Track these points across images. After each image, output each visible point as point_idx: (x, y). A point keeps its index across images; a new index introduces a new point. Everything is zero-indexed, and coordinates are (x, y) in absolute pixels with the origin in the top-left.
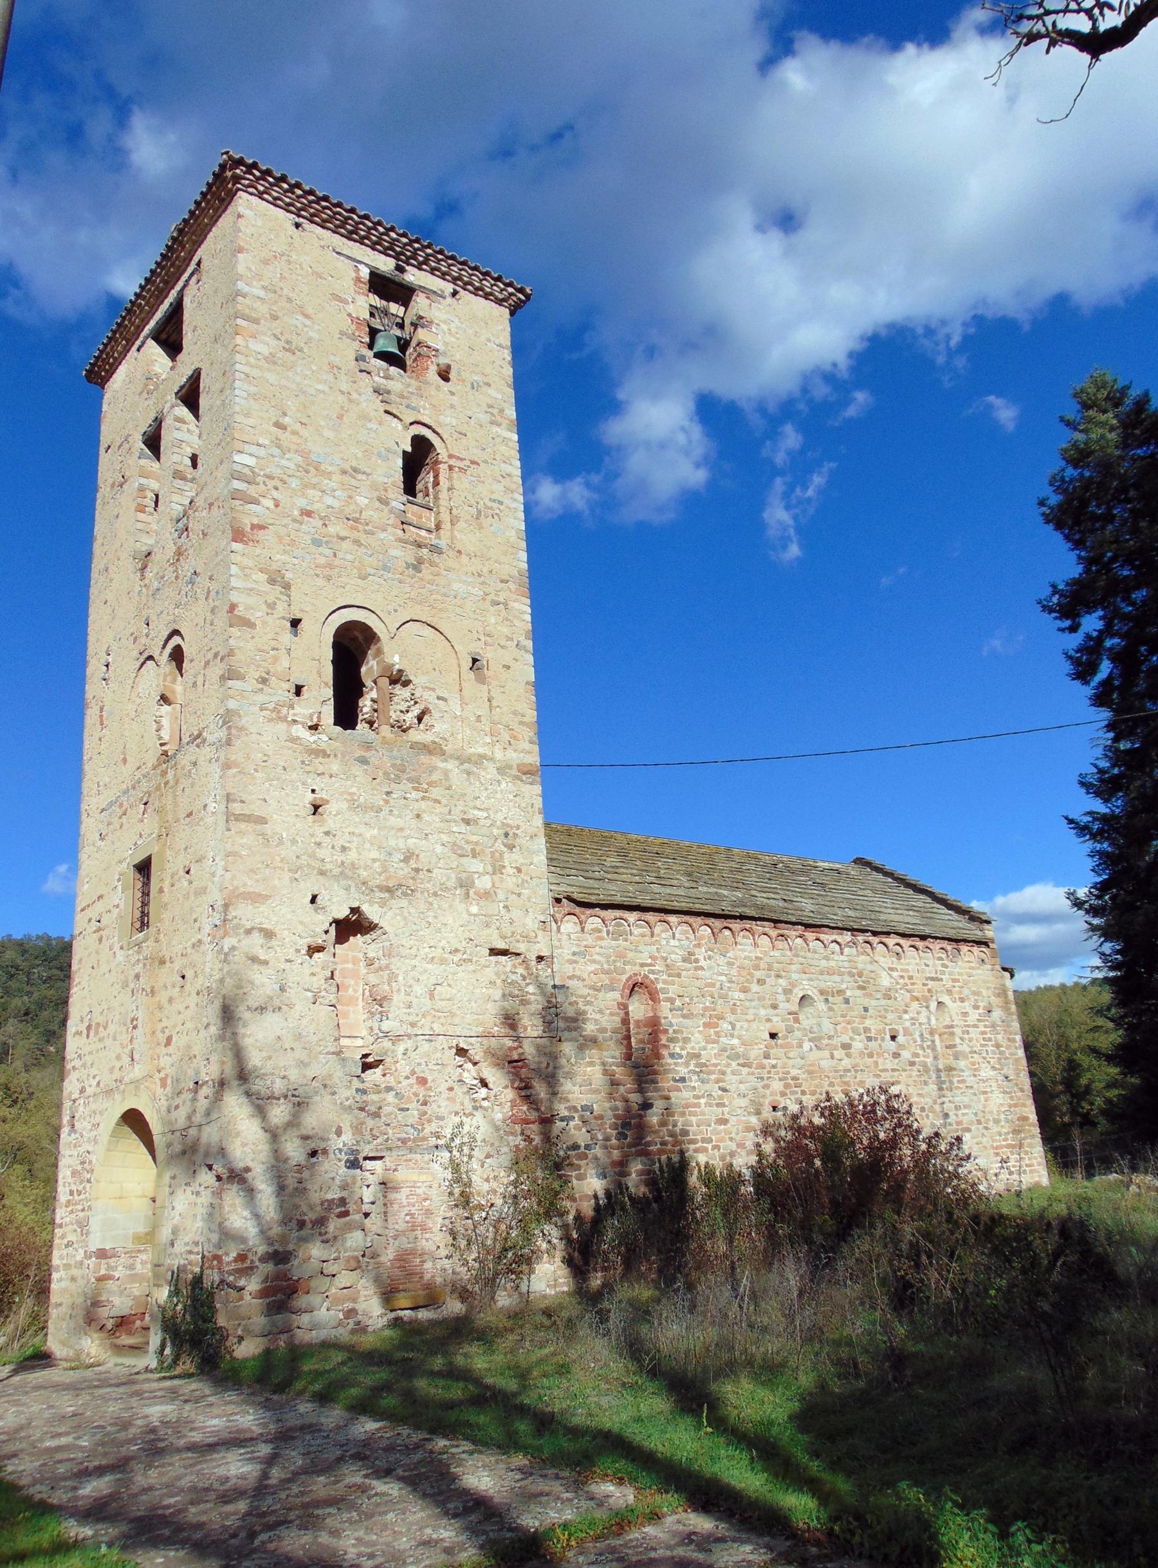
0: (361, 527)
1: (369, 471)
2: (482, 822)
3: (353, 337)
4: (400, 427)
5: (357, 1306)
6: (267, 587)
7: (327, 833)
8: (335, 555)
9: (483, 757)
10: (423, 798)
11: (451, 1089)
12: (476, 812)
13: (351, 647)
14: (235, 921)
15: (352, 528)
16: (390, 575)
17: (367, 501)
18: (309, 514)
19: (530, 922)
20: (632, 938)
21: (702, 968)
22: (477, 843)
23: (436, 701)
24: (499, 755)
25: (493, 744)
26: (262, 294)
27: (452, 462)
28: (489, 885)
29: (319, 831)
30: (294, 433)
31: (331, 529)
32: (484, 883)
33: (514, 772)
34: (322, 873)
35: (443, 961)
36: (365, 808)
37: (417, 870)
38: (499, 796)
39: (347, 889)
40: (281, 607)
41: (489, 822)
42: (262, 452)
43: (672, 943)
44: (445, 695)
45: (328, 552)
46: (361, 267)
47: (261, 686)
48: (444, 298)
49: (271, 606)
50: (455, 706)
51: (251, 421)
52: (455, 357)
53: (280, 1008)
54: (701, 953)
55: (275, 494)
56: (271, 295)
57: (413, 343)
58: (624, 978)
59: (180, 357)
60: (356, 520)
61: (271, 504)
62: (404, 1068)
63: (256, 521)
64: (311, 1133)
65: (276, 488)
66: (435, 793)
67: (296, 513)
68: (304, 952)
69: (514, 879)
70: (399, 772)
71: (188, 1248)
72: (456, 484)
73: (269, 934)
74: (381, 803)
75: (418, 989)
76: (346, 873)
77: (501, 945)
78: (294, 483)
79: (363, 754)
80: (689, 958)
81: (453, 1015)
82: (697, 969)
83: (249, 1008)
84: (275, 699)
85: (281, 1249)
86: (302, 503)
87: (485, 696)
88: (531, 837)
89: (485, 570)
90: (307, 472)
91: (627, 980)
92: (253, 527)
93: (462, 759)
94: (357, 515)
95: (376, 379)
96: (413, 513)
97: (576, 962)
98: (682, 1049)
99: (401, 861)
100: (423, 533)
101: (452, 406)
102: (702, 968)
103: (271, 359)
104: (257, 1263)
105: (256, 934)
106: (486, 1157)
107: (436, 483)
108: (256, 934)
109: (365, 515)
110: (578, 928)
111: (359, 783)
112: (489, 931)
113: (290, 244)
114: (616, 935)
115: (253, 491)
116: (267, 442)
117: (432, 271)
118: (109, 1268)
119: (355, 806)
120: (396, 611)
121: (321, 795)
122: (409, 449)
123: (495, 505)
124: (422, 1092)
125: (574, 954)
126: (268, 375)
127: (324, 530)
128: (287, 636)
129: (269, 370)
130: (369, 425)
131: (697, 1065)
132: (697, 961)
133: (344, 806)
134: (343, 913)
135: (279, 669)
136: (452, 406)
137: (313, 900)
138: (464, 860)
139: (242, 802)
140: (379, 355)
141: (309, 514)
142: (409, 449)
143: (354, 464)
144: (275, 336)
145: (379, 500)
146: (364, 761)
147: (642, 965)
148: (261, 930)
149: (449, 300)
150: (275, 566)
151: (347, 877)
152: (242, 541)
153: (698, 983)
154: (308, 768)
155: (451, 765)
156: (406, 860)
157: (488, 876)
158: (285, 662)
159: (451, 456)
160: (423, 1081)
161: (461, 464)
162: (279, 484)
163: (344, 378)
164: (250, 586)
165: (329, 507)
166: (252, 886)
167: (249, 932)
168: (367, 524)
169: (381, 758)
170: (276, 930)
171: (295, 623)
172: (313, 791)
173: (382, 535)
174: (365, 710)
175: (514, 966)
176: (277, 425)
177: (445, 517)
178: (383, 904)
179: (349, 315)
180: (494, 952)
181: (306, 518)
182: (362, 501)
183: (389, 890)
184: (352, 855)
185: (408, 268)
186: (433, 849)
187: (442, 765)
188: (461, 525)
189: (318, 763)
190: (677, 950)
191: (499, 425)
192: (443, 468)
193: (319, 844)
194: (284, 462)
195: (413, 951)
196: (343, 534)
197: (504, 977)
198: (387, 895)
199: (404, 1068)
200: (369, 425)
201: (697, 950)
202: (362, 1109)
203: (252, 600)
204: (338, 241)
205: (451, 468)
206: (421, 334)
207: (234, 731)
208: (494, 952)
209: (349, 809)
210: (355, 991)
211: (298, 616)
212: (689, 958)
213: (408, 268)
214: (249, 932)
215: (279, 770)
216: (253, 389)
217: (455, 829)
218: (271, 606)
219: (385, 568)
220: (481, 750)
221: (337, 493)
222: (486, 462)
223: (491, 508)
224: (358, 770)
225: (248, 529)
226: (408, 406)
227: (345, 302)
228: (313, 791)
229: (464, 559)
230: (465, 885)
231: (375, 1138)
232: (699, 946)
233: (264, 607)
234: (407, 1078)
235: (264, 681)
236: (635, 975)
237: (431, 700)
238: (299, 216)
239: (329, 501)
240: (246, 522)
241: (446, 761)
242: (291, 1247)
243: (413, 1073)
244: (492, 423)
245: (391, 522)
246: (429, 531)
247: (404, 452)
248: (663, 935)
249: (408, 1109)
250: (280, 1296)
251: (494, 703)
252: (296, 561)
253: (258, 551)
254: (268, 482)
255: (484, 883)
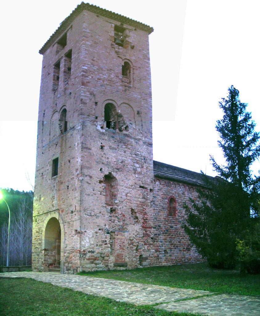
0: (112, 82)
1: (114, 70)
2: (139, 155)
3: (111, 40)
4: (121, 60)
5: (108, 264)
6: (90, 96)
7: (104, 154)
8: (106, 88)
9: (140, 139)
10: (126, 148)
11: (130, 218)
12: (138, 152)
13: (109, 109)
14: (83, 173)
15: (110, 82)
16: (119, 93)
17: (113, 76)
18: (100, 79)
19: (149, 181)
20: (171, 187)
21: (186, 196)
22: (138, 160)
23: (130, 124)
24: (143, 139)
25: (142, 136)
26: (89, 31)
27: (134, 68)
28: (140, 171)
29: (102, 153)
30: (97, 62)
31: (105, 83)
32: (139, 170)
33: (147, 144)
34: (103, 163)
35: (129, 188)
36: (113, 148)
37: (124, 165)
38: (143, 149)
39: (109, 168)
40: (93, 100)
41: (141, 155)
42: (89, 66)
43: (180, 189)
44: (132, 123)
45: (104, 88)
46: (112, 24)
47: (88, 117)
48: (132, 30)
49: (91, 99)
50: (134, 126)
51: (86, 59)
52: (134, 44)
53: (93, 195)
54: (186, 193)
55: (92, 75)
56: (91, 32)
57: (125, 41)
58: (169, 197)
59: (71, 49)
60: (111, 81)
61: (91, 77)
62: (120, 212)
63: (87, 81)
64: (99, 225)
65: (92, 74)
66: (129, 147)
67: (97, 79)
68: (98, 182)
69: (146, 170)
70: (120, 141)
71: (70, 248)
72: (135, 72)
73: (91, 177)
74: (117, 148)
75: (124, 194)
76: (108, 164)
77: (142, 185)
78: (96, 73)
79: (113, 135)
80: (183, 194)
81: (131, 200)
82: (185, 196)
83: (86, 194)
84: (91, 119)
85: (93, 250)
86: (98, 77)
87: (141, 124)
88: (150, 160)
89: (141, 92)
90: (99, 70)
91: (170, 197)
92: (87, 82)
93: (135, 139)
94: (111, 80)
95: (116, 49)
96: (124, 79)
97: (159, 192)
98: (180, 215)
99: (120, 162)
100: (126, 84)
101: (134, 55)
102: (186, 196)
103: (91, 46)
104: (88, 253)
105: (88, 177)
106: (137, 235)
107: (130, 72)
108: (88, 177)
109: (113, 79)
110: (159, 183)
111: (112, 143)
112: (140, 182)
113: (96, 20)
114: (168, 186)
115: (87, 75)
116: (90, 64)
117: (130, 25)
118: (47, 253)
119: (111, 148)
120: (120, 101)
121: (104, 144)
122: (123, 65)
123: (145, 77)
124: (124, 218)
125: (158, 189)
126: (90, 49)
127: (103, 83)
128: (94, 106)
129: (90, 48)
130: (114, 60)
131: (183, 219)
132: (185, 194)
133: (108, 147)
134: (107, 173)
135: (92, 113)
136: (134, 55)
137: (101, 170)
138: (135, 164)
139: (85, 144)
140: (117, 44)
141: (100, 79)
142: (123, 65)
143: (110, 68)
144: (92, 40)
145: (117, 76)
146: (113, 137)
147: (173, 194)
148: (89, 176)
149: (134, 31)
150: (92, 91)
151: (109, 165)
152: (84, 85)
153: (185, 200)
154: (100, 137)
155: (133, 140)
156: (122, 162)
157: (140, 168)
158: (94, 112)
159: (133, 66)
160: (124, 216)
161: (136, 68)
162: (93, 73)
163: (108, 49)
164: (86, 95)
165: (104, 78)
166: (87, 165)
167: (86, 176)
168: (113, 82)
169: (118, 137)
170: (92, 176)
171: (96, 103)
172: (101, 143)
173: (117, 84)
174: (112, 125)
175: (145, 191)
176: (93, 60)
177: (132, 80)
178: (116, 172)
179: (110, 35)
180: (141, 187)
181: (99, 80)
182: (112, 76)
183: (118, 169)
184: (110, 160)
185: (124, 24)
186: (129, 160)
187: (130, 140)
188: (136, 82)
189: (103, 137)
190: (181, 191)
191: (146, 59)
192: (131, 69)
193: (102, 156)
194: (94, 68)
195: (123, 185)
196: (108, 84)
197: (142, 193)
198: (117, 170)
199: (120, 212)
200: (114, 60)
201: (185, 192)
202: (110, 221)
203: (87, 98)
204: (107, 19)
205: (134, 69)
206: (127, 39)
207: (84, 127)
208: (141, 187)
209: (109, 148)
210: (108, 193)
211: (97, 102)
212: (183, 194)
213: (124, 24)
214: (86, 176)
215: (94, 137)
216: (87, 52)
217: (133, 156)
218: (91, 99)
219: (117, 91)
220: (140, 138)
221: (107, 75)
222: (142, 67)
223: (143, 78)
224: (111, 139)
225: (85, 83)
226: (123, 55)
227: (109, 33)
228: (101, 143)
229: (136, 89)
230: (135, 170)
231: (113, 227)
232: (186, 191)
233: (89, 100)
234: (120, 214)
235: (89, 116)
236: (171, 196)
237: (128, 124)
238: (98, 14)
239: (105, 76)
240: (85, 81)
241: (131, 139)
242: (95, 250)
243: (122, 213)
244: (144, 59)
245: (119, 81)
246: (128, 83)
247: (122, 66)
248: (178, 187)
249: (120, 222)
250: (92, 260)
251: (143, 126)
252: (96, 90)
253: (88, 88)
254: (90, 72)
255: (139, 170)
